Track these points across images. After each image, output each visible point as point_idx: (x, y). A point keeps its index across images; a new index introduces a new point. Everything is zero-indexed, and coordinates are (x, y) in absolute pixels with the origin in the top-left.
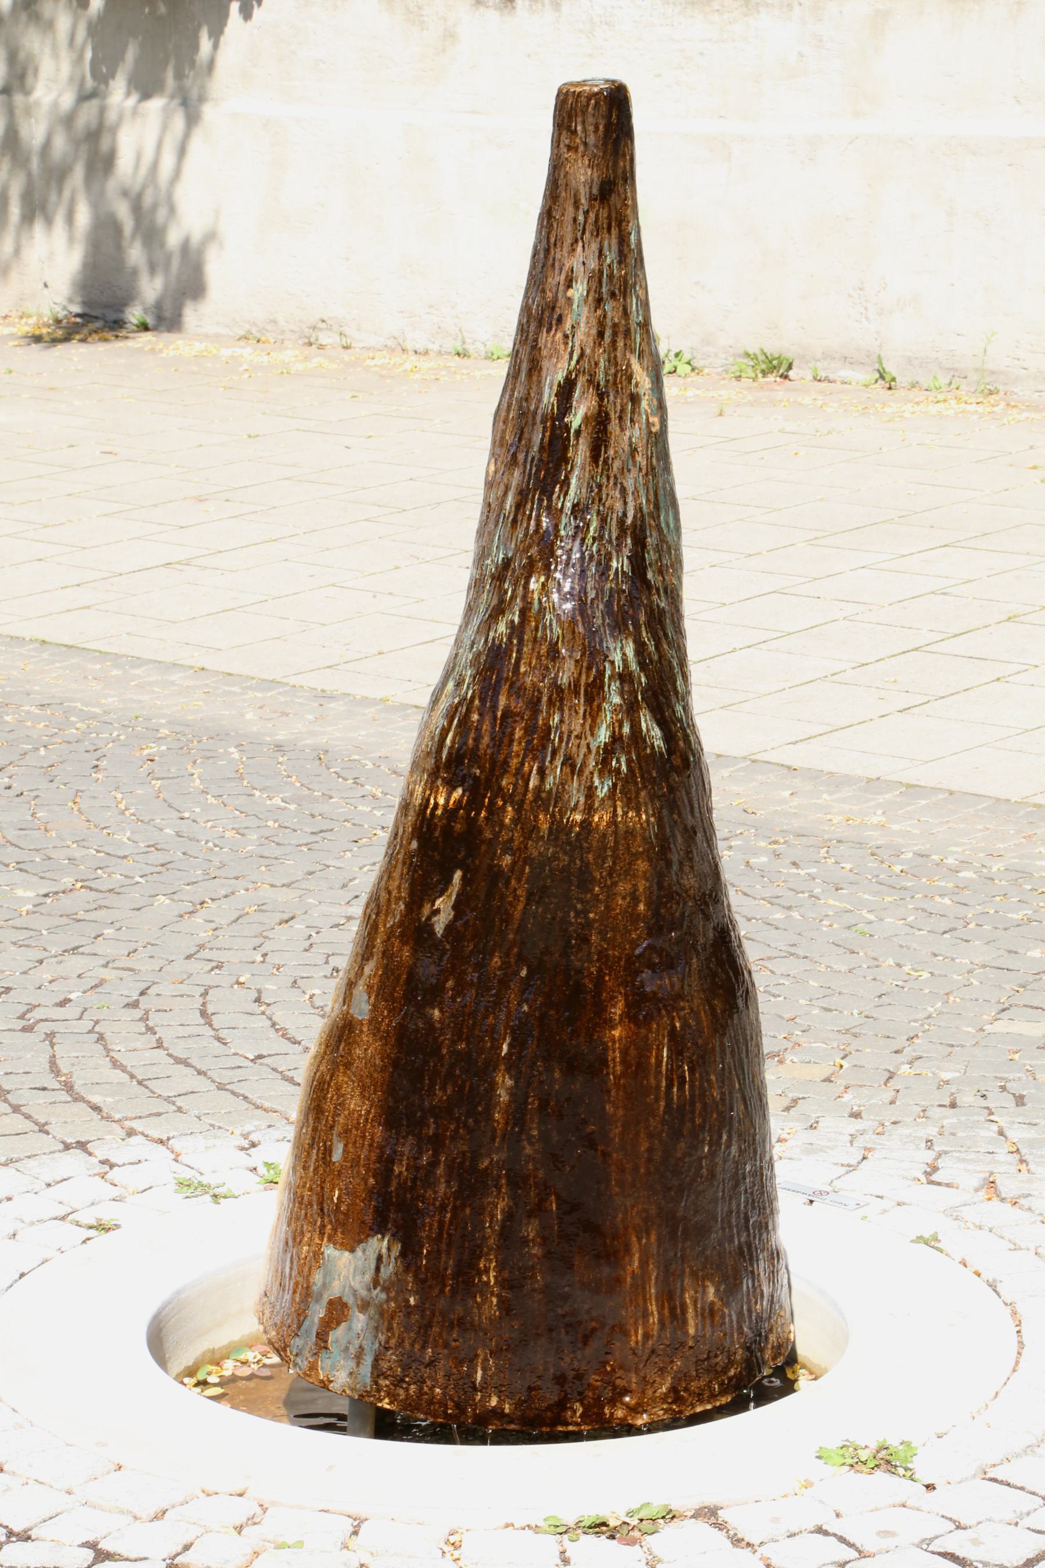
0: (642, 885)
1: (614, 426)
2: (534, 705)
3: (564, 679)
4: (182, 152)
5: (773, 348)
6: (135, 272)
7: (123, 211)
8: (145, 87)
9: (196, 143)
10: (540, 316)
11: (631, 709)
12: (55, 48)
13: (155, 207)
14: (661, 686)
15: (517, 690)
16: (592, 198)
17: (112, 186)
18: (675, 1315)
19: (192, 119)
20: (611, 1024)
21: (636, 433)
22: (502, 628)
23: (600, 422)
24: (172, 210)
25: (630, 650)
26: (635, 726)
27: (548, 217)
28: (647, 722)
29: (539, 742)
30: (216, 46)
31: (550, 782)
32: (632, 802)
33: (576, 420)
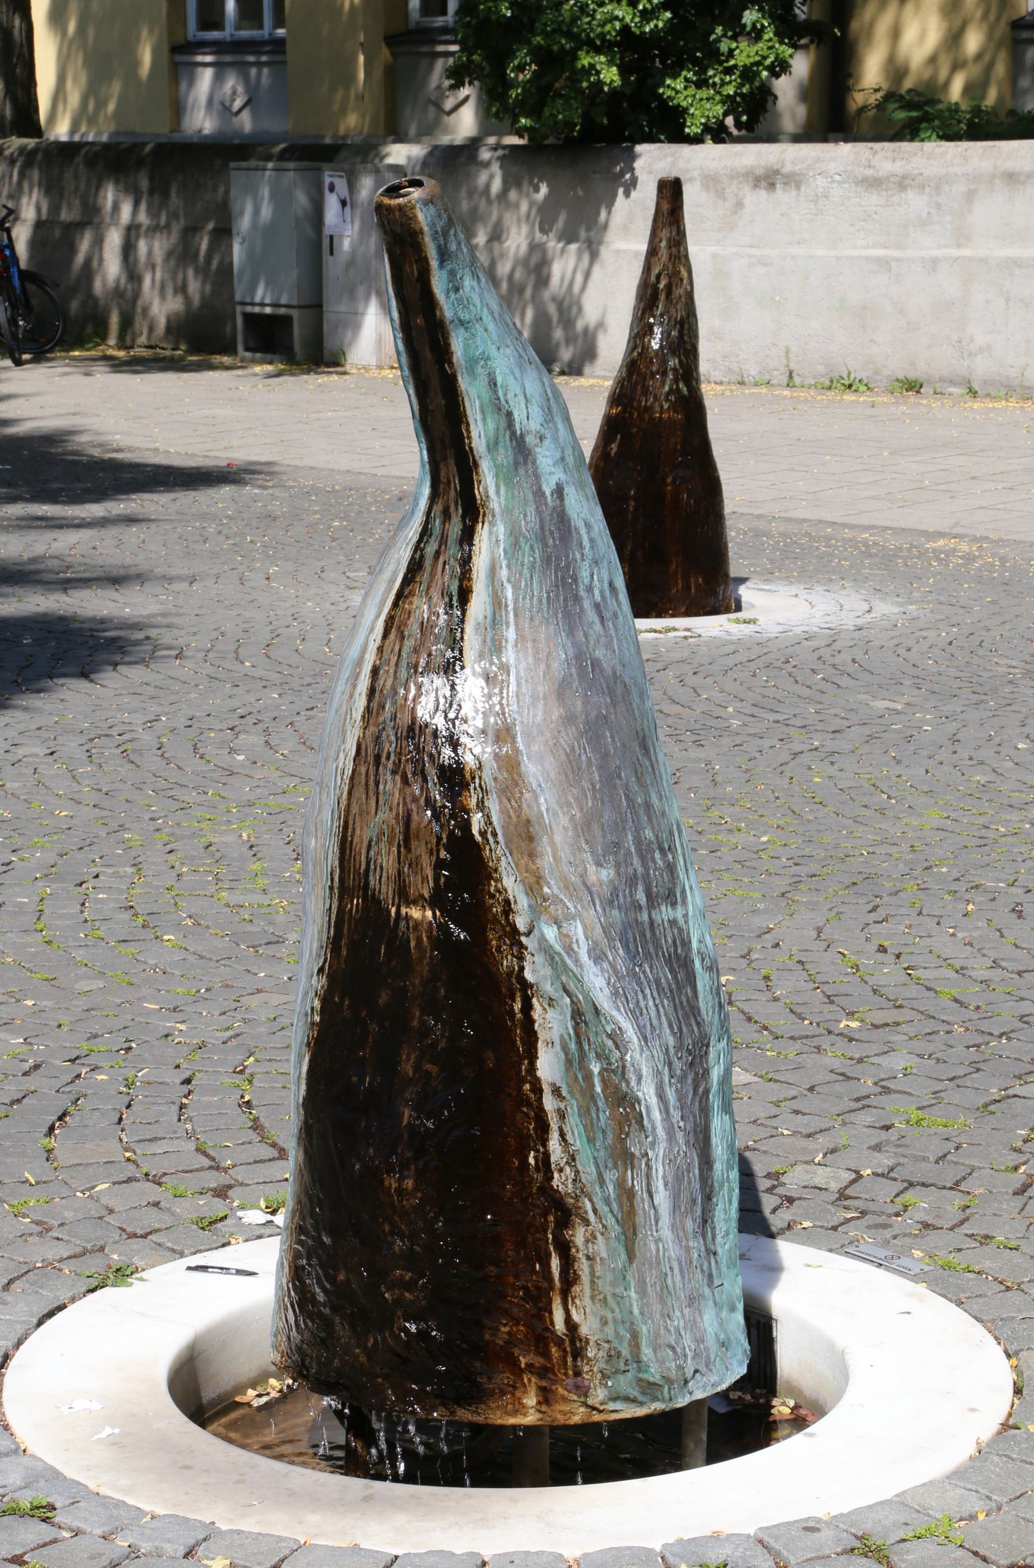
0: (679, 440)
1: (674, 288)
2: (644, 378)
3: (654, 369)
4: (587, 275)
5: (912, 375)
6: (558, 345)
7: (552, 310)
8: (568, 237)
9: (597, 271)
10: (652, 252)
11: (676, 380)
12: (519, 221)
13: (570, 307)
14: (689, 373)
15: (639, 374)
16: (668, 214)
17: (546, 295)
18: (687, 587)
19: (594, 256)
20: (667, 485)
21: (681, 291)
22: (635, 354)
23: (669, 288)
24: (580, 309)
25: (677, 361)
26: (678, 386)
27: (655, 220)
28: (681, 385)
29: (646, 392)
30: (609, 213)
31: (649, 404)
32: (675, 412)
33: (661, 286)
